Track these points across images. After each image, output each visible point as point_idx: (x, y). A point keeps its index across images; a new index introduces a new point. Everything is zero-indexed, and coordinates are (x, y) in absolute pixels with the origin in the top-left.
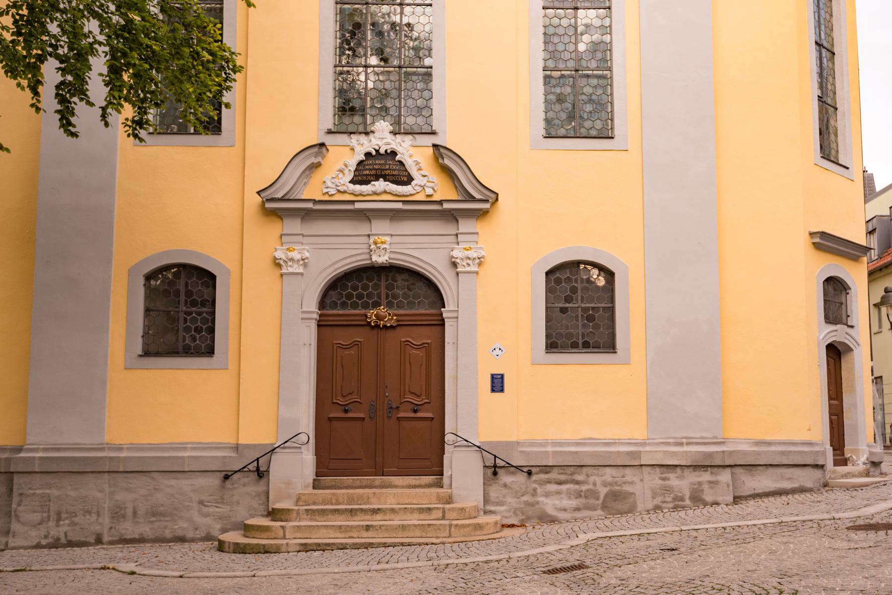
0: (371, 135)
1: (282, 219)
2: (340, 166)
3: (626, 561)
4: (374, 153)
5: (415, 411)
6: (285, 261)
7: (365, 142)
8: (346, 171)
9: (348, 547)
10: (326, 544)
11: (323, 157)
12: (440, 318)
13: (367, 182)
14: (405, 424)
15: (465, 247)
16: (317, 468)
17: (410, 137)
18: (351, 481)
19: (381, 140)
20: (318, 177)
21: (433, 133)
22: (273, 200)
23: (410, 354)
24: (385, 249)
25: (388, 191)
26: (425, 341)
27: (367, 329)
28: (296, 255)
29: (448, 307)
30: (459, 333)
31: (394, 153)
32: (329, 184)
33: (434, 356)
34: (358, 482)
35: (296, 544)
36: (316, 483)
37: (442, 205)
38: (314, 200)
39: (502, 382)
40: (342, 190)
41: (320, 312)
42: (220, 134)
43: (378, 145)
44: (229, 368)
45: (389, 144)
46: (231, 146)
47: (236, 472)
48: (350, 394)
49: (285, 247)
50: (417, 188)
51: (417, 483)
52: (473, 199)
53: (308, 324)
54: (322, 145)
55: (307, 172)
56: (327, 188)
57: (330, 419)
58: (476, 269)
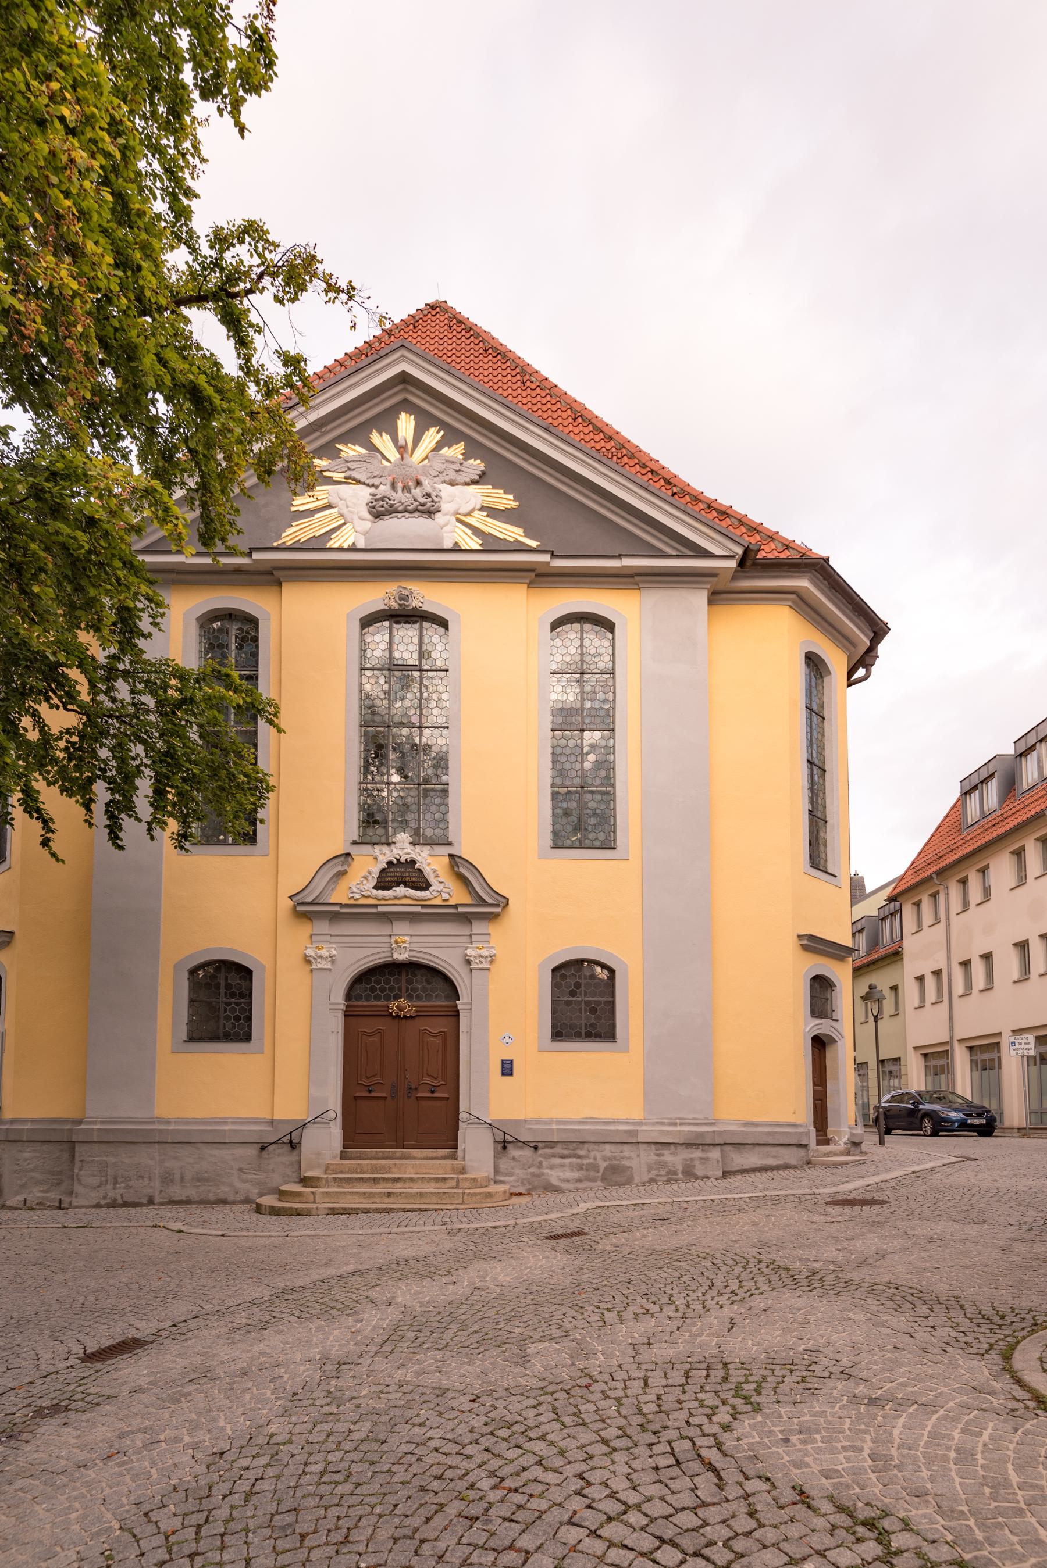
0: (393, 846)
2: (364, 873)
3: (621, 1229)
4: (395, 861)
5: (432, 1092)
8: (370, 878)
11: (349, 865)
13: (388, 888)
17: (428, 847)
21: (450, 844)
28: (324, 953)
31: (413, 862)
32: (355, 890)
45: (409, 853)
51: (434, 1155)
52: (485, 903)
54: (348, 855)
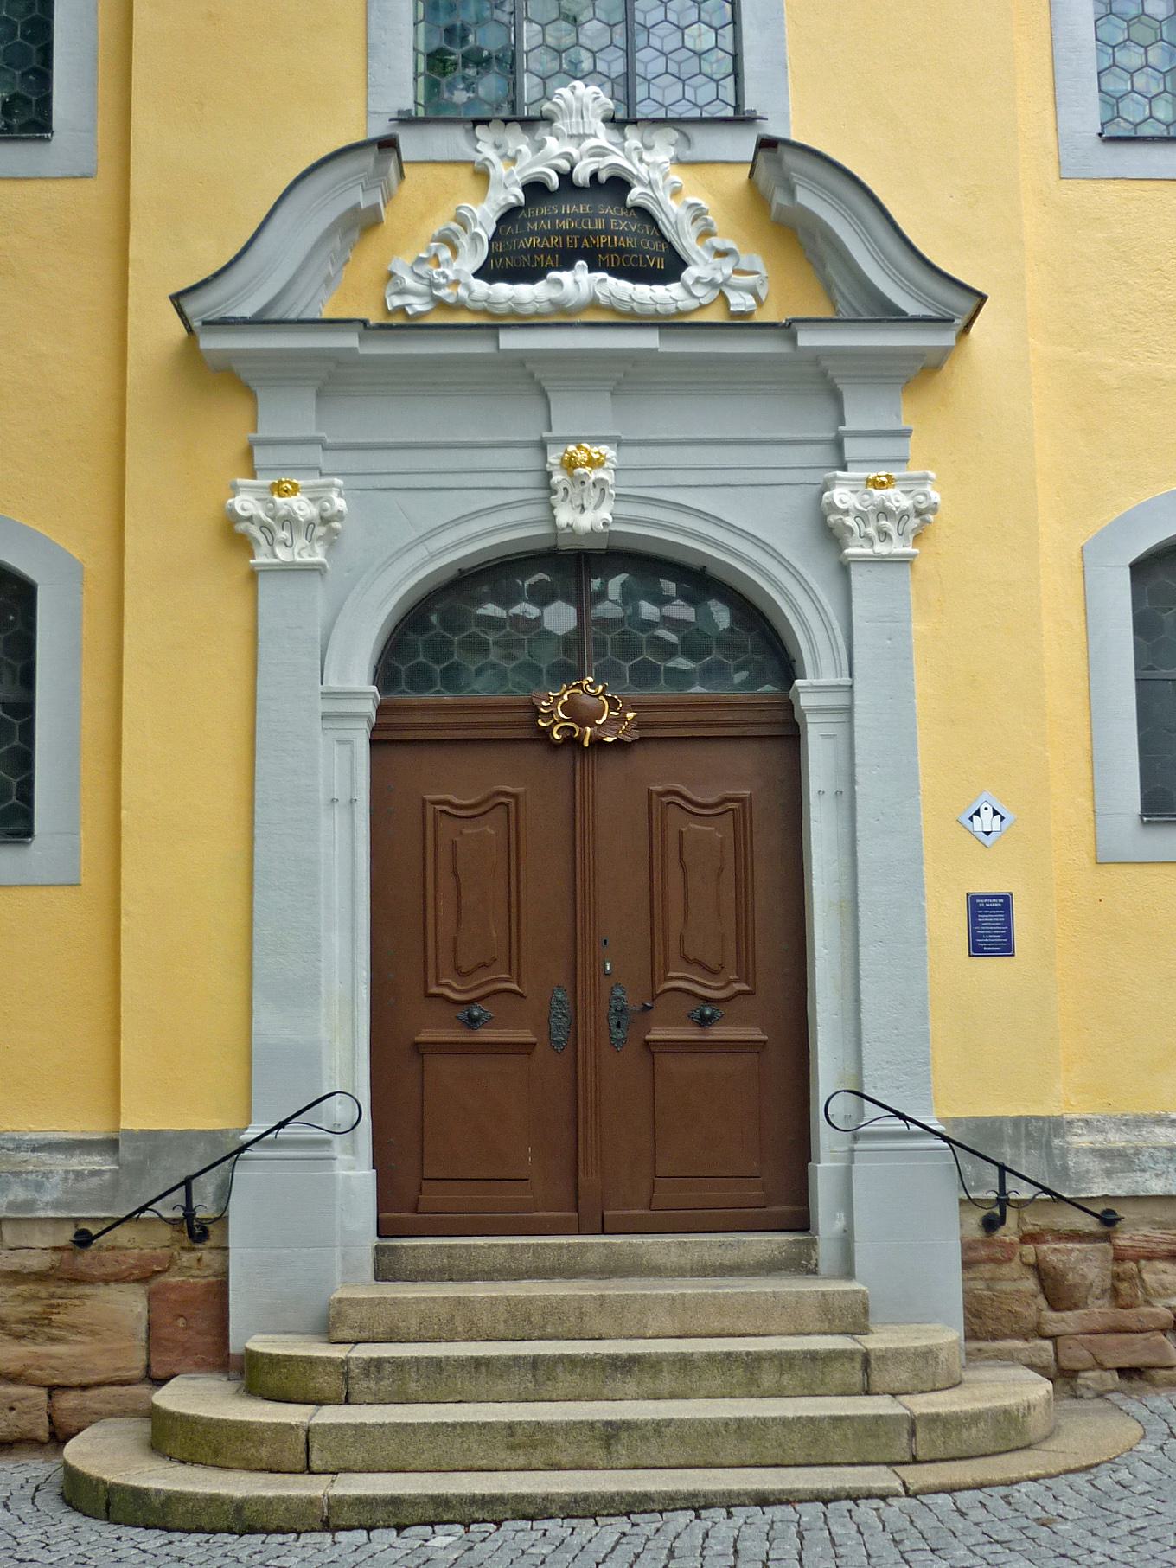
0: (542, 132)
1: (249, 393)
2: (441, 222)
5: (704, 1022)
6: (264, 527)
7: (524, 148)
8: (464, 241)
9: (554, 1510)
10: (473, 1500)
12: (781, 716)
13: (531, 274)
14: (668, 1063)
15: (872, 475)
16: (808, 1212)
17: (672, 134)
19: (575, 141)
20: (367, 261)
22: (225, 323)
23: (681, 833)
24: (600, 484)
25: (603, 301)
26: (731, 793)
27: (536, 751)
28: (301, 506)
29: (816, 676)
30: (858, 759)
31: (619, 184)
32: (409, 282)
33: (766, 840)
34: (528, 1256)
36: (385, 1259)
37: (794, 339)
38: (364, 322)
40: (451, 300)
42: (48, 140)
43: (567, 156)
44: (83, 880)
45: (600, 152)
46: (84, 177)
47: (120, 1222)
48: (484, 965)
49: (264, 481)
50: (699, 291)
51: (730, 1257)
52: (890, 315)
53: (345, 736)
55: (336, 243)
57: (420, 1049)
58: (909, 550)
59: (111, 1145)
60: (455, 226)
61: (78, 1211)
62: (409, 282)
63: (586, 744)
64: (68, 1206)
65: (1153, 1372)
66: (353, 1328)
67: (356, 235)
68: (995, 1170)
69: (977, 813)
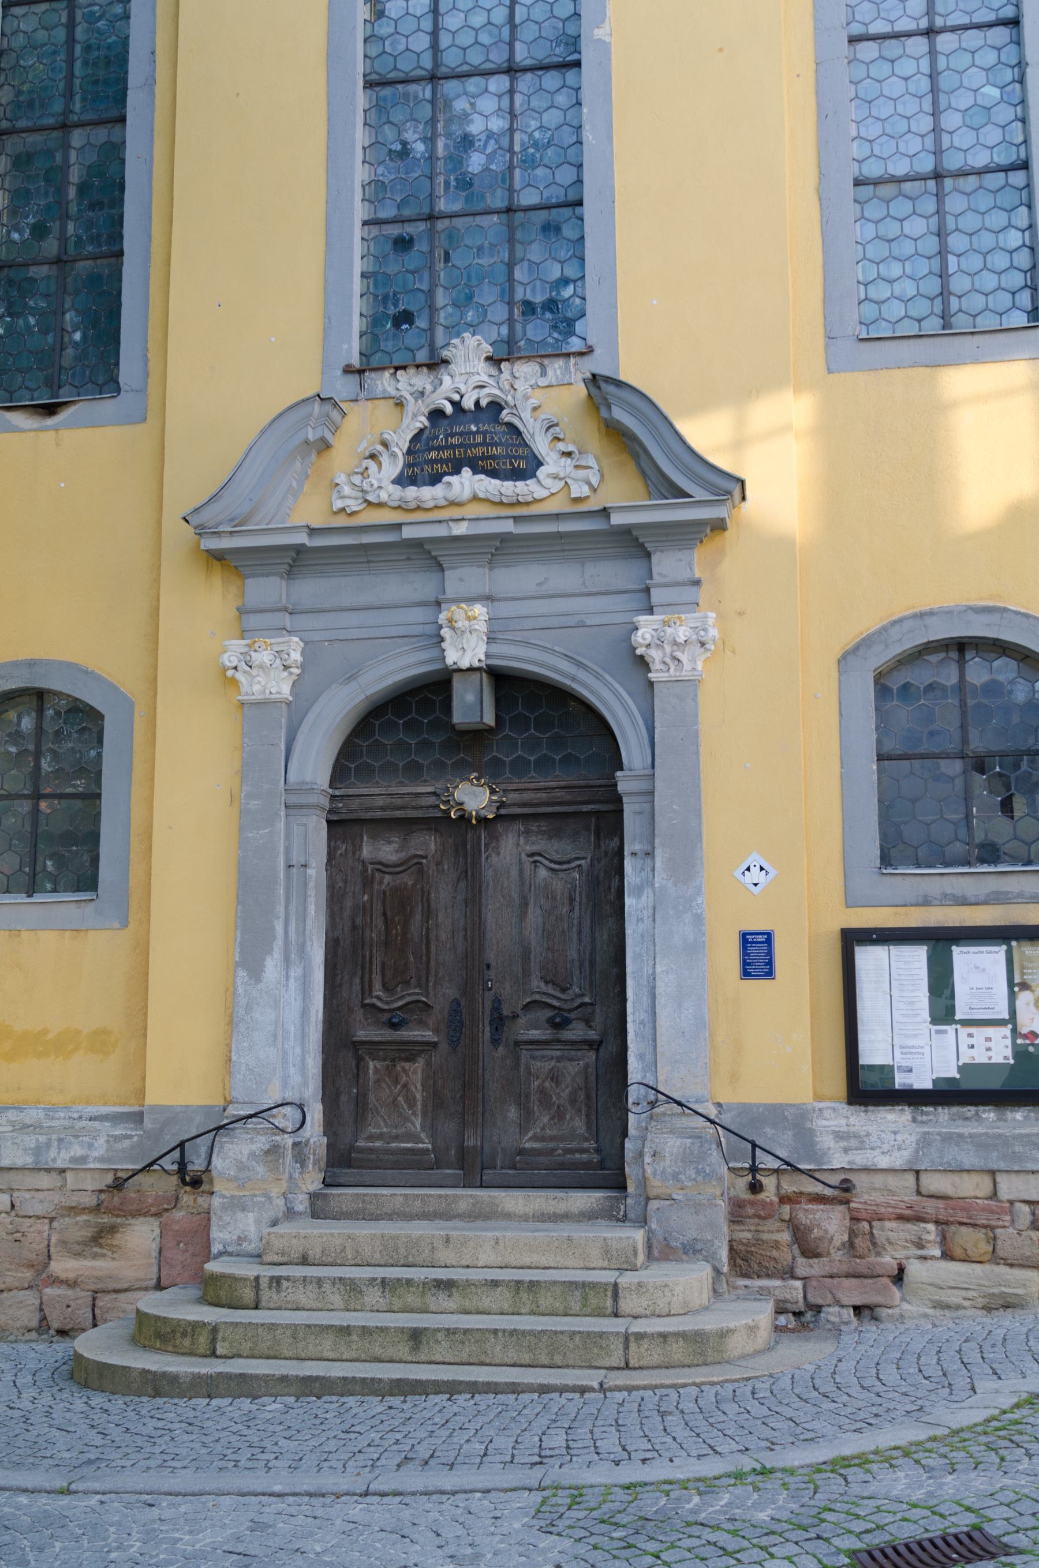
4: (449, 409)
8: (385, 459)
13: (435, 480)
18: (401, 1199)
25: (481, 495)
34: (418, 1203)
35: (402, 1330)
39: (770, 953)
41: (330, 791)
51: (561, 1207)
56: (343, 497)
59: (138, 1118)
60: (380, 448)
61: (118, 1164)
62: (347, 490)
63: (474, 822)
64: (109, 1160)
65: (879, 1309)
66: (277, 1254)
67: (314, 457)
68: (749, 1146)
69: (748, 869)
